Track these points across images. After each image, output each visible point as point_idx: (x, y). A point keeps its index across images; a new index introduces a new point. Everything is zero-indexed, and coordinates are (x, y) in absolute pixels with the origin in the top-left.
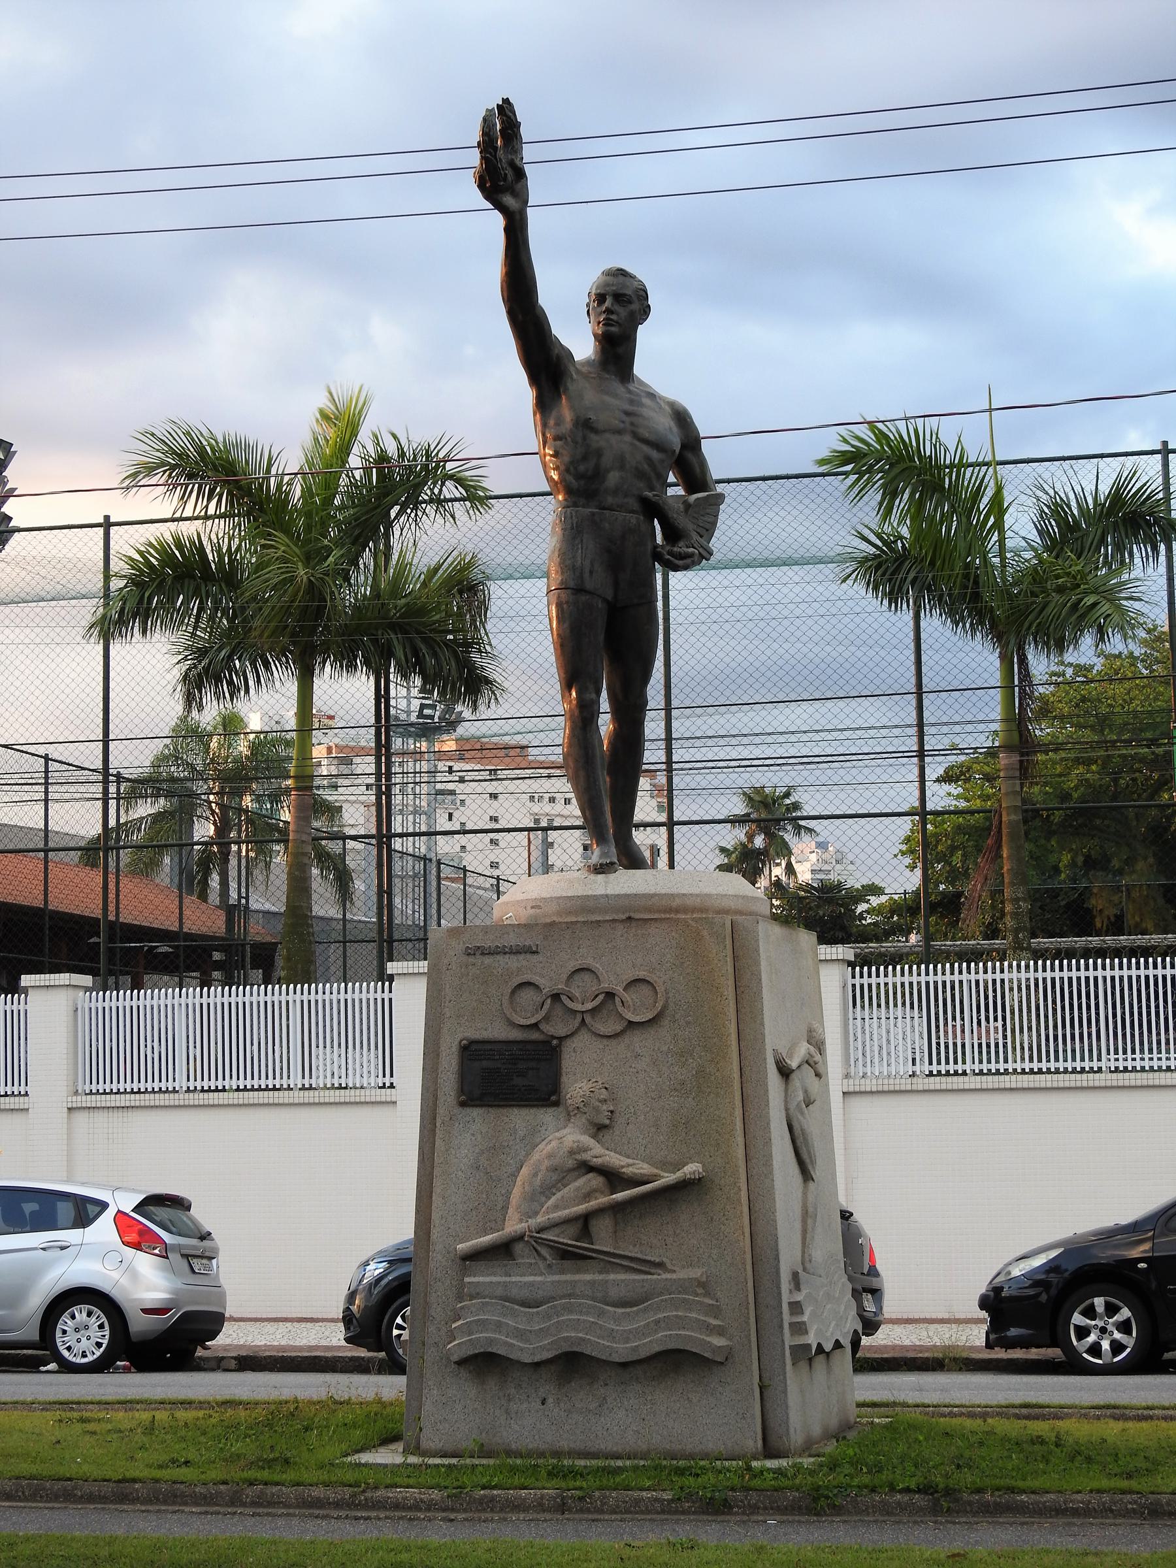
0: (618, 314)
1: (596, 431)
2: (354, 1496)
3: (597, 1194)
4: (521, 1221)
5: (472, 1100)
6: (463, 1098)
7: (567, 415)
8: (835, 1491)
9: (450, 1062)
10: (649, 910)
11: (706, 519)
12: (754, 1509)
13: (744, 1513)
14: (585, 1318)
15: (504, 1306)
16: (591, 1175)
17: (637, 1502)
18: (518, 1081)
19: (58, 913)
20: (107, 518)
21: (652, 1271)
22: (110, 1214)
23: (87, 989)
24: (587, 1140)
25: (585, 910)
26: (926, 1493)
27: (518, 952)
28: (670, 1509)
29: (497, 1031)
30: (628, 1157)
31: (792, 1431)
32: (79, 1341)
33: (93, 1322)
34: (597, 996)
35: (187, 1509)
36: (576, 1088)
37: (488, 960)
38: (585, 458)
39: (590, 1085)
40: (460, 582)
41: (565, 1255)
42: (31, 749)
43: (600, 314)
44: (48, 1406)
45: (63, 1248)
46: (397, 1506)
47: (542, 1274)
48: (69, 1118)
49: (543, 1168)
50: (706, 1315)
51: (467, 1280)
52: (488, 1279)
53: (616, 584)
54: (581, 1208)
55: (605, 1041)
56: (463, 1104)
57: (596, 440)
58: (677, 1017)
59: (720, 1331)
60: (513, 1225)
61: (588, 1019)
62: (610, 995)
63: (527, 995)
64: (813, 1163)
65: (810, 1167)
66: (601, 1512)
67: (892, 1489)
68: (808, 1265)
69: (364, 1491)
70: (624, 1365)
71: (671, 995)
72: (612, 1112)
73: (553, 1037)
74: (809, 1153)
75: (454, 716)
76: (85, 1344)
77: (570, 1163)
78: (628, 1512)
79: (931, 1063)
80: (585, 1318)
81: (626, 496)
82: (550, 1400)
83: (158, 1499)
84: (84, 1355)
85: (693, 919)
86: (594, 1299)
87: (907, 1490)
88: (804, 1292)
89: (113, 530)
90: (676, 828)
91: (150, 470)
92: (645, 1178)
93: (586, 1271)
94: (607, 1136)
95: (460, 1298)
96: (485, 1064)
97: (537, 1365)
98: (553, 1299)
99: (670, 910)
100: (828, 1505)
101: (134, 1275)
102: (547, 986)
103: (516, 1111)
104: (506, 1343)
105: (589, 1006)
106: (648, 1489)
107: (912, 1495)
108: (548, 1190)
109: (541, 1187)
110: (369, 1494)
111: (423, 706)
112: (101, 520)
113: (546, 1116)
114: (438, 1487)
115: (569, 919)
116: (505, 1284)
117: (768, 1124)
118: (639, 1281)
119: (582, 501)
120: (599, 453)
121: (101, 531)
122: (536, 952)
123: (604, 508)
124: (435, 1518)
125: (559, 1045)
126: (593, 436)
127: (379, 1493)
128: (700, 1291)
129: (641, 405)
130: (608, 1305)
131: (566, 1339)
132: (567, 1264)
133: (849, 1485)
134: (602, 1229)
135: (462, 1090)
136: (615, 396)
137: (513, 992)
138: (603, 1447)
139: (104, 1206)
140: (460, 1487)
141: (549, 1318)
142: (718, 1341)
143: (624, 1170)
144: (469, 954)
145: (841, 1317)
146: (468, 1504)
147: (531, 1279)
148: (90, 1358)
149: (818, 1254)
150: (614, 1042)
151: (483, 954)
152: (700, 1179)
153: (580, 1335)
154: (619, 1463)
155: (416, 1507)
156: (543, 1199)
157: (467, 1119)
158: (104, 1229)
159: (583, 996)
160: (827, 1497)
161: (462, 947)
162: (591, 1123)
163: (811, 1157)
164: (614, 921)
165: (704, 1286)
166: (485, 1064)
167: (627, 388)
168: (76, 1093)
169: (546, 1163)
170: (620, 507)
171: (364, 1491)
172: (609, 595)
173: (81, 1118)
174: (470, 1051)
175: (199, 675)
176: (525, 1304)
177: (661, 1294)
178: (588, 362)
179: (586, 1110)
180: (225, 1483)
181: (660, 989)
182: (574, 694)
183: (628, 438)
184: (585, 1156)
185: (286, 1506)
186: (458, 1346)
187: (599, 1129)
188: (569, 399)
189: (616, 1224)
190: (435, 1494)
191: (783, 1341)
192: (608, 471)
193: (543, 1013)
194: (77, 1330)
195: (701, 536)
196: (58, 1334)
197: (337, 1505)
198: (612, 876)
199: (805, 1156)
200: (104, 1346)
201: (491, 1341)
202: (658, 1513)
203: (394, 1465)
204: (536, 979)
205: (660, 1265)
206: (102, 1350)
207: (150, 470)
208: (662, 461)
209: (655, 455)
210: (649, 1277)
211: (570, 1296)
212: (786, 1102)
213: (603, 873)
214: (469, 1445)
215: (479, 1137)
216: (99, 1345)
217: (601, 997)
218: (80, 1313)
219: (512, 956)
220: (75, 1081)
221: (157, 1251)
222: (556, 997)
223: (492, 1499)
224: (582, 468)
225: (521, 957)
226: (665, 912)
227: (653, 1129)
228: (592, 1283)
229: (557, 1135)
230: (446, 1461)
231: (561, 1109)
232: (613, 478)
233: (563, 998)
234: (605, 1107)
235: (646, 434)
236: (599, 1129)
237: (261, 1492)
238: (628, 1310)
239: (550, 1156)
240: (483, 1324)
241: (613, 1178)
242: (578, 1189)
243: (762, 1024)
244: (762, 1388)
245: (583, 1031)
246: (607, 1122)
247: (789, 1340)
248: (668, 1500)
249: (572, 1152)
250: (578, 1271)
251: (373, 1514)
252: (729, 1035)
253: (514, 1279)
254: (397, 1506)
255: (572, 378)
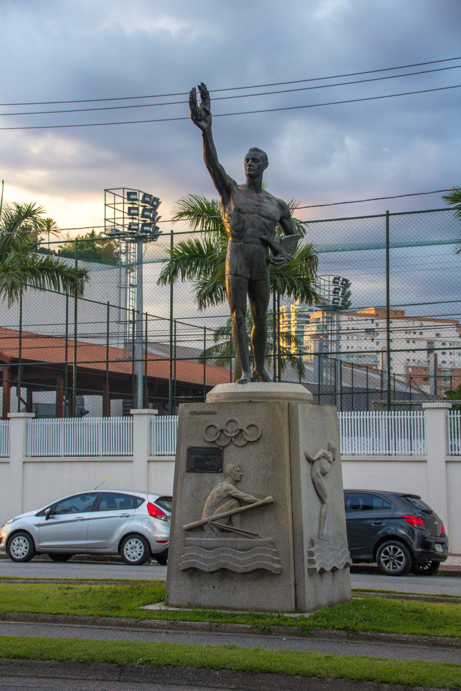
0: (253, 166)
1: (243, 213)
2: (136, 622)
3: (234, 507)
4: (207, 517)
5: (191, 470)
6: (188, 469)
7: (233, 207)
8: (311, 628)
9: (184, 455)
10: (258, 398)
11: (291, 245)
12: (280, 633)
13: (276, 635)
14: (228, 555)
15: (200, 549)
16: (232, 500)
17: (238, 628)
18: (207, 463)
19: (180, 382)
20: (172, 231)
21: (254, 537)
22: (146, 503)
23: (156, 415)
24: (231, 486)
25: (234, 398)
26: (345, 630)
27: (209, 414)
28: (249, 632)
29: (201, 444)
30: (247, 493)
31: (307, 602)
32: (132, 553)
33: (138, 546)
34: (236, 431)
35: (76, 626)
36: (228, 466)
37: (198, 416)
38: (238, 224)
39: (233, 465)
40: (306, 255)
41: (223, 530)
42: (157, 318)
43: (247, 167)
44: (52, 581)
45: (127, 516)
46: (151, 627)
47: (214, 537)
48: (148, 465)
49: (215, 496)
50: (273, 555)
51: (187, 539)
52: (194, 539)
53: (251, 272)
54: (228, 512)
55: (239, 448)
56: (188, 471)
57: (244, 217)
58: (266, 439)
59: (278, 562)
60: (204, 518)
61: (233, 440)
62: (241, 431)
63: (212, 430)
64: (325, 496)
65: (324, 498)
66: (224, 632)
67: (333, 628)
68: (320, 537)
69: (140, 620)
70: (244, 574)
71: (264, 431)
72: (241, 476)
73: (221, 446)
74: (323, 493)
75: (347, 303)
76: (135, 554)
77: (225, 495)
78: (234, 632)
79: (452, 450)
80: (228, 555)
81: (254, 238)
82: (216, 587)
83: (67, 621)
84: (134, 558)
85: (273, 402)
86: (232, 547)
87: (339, 629)
88: (315, 547)
89: (174, 236)
90: (391, 353)
91: (181, 215)
92: (252, 502)
93: (230, 537)
94: (239, 485)
95: (185, 546)
96: (196, 456)
97: (212, 572)
98: (217, 547)
99: (266, 398)
100: (308, 633)
101: (154, 528)
102: (219, 426)
103: (207, 474)
104: (199, 564)
105: (233, 435)
106: (243, 623)
107: (340, 631)
108: (217, 505)
109: (214, 504)
110: (141, 622)
111: (334, 299)
112: (170, 232)
113: (218, 476)
114: (167, 620)
115: (228, 401)
116: (200, 541)
117: (300, 481)
118: (249, 541)
119: (238, 240)
120: (244, 221)
121: (170, 236)
122: (215, 414)
123: (246, 243)
124: (163, 632)
125: (223, 450)
126: (242, 215)
127: (145, 621)
128: (272, 546)
129: (263, 202)
130: (237, 550)
131: (221, 563)
132: (223, 534)
133: (317, 626)
134: (236, 520)
135: (187, 466)
136: (252, 199)
137: (207, 429)
138: (235, 606)
139: (143, 500)
140: (175, 620)
141: (216, 554)
142: (277, 566)
143: (244, 498)
144: (191, 414)
145: (339, 558)
146: (176, 627)
147: (210, 539)
148: (136, 560)
149: (328, 531)
150: (243, 449)
151: (196, 414)
152: (272, 503)
153: (227, 562)
154: (237, 612)
155: (158, 627)
156: (215, 508)
157: (189, 477)
158: (143, 510)
159: (231, 432)
160: (308, 630)
161: (189, 411)
162: (233, 479)
163: (324, 494)
164: (244, 402)
165: (272, 544)
166: (196, 456)
167: (258, 196)
168: (151, 455)
169: (216, 495)
170: (252, 243)
171: (140, 620)
172: (249, 276)
173: (153, 465)
174: (191, 451)
175: (204, 294)
176: (207, 549)
177: (257, 546)
178: (243, 186)
179: (231, 474)
180: (92, 616)
181: (260, 428)
182: (234, 314)
183: (256, 215)
184: (230, 492)
185: (112, 625)
186: (184, 564)
187: (236, 482)
188: (233, 200)
189: (242, 519)
190: (165, 622)
191: (304, 567)
192: (247, 229)
193: (217, 437)
194: (132, 548)
195: (288, 252)
196: (125, 550)
197: (130, 625)
198: (245, 385)
199: (321, 494)
200: (142, 555)
201: (194, 563)
202: (245, 633)
203: (155, 610)
204: (215, 424)
205: (257, 535)
206: (141, 556)
207: (181, 215)
208: (271, 224)
209: (267, 221)
210: (253, 540)
211: (223, 546)
212: (311, 473)
213: (242, 383)
214: (186, 603)
215: (193, 484)
216: (140, 554)
217: (238, 431)
218: (133, 542)
219: (207, 415)
220: (151, 450)
221: (163, 518)
222: (222, 431)
223: (185, 625)
224: (237, 227)
225: (210, 415)
226: (264, 399)
227: (256, 483)
228: (232, 542)
229: (221, 484)
230: (175, 609)
231: (223, 474)
232: (249, 231)
233: (225, 431)
234: (238, 474)
235: (264, 214)
236: (236, 482)
237: (104, 620)
238: (244, 552)
239: (218, 492)
240: (192, 556)
241: (240, 501)
242: (227, 505)
243: (299, 443)
244: (296, 585)
245: (232, 444)
246: (239, 479)
247: (307, 566)
248: (249, 628)
249: (226, 491)
250: (227, 537)
251: (141, 630)
252: (285, 447)
253: (204, 539)
254: (151, 627)
255: (235, 192)
